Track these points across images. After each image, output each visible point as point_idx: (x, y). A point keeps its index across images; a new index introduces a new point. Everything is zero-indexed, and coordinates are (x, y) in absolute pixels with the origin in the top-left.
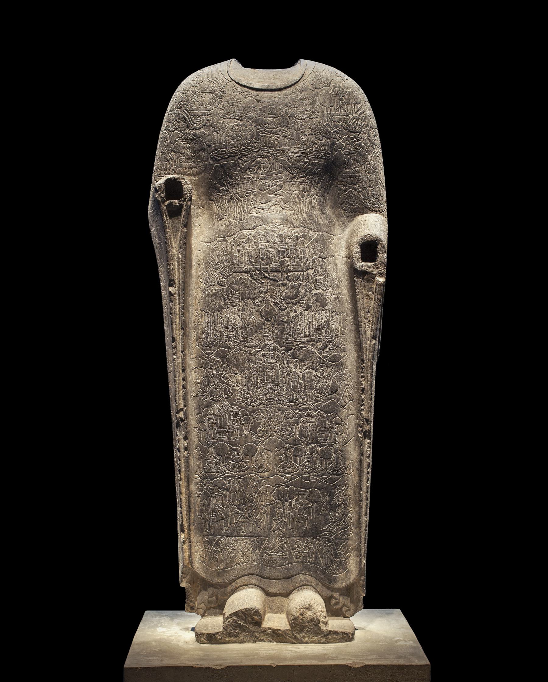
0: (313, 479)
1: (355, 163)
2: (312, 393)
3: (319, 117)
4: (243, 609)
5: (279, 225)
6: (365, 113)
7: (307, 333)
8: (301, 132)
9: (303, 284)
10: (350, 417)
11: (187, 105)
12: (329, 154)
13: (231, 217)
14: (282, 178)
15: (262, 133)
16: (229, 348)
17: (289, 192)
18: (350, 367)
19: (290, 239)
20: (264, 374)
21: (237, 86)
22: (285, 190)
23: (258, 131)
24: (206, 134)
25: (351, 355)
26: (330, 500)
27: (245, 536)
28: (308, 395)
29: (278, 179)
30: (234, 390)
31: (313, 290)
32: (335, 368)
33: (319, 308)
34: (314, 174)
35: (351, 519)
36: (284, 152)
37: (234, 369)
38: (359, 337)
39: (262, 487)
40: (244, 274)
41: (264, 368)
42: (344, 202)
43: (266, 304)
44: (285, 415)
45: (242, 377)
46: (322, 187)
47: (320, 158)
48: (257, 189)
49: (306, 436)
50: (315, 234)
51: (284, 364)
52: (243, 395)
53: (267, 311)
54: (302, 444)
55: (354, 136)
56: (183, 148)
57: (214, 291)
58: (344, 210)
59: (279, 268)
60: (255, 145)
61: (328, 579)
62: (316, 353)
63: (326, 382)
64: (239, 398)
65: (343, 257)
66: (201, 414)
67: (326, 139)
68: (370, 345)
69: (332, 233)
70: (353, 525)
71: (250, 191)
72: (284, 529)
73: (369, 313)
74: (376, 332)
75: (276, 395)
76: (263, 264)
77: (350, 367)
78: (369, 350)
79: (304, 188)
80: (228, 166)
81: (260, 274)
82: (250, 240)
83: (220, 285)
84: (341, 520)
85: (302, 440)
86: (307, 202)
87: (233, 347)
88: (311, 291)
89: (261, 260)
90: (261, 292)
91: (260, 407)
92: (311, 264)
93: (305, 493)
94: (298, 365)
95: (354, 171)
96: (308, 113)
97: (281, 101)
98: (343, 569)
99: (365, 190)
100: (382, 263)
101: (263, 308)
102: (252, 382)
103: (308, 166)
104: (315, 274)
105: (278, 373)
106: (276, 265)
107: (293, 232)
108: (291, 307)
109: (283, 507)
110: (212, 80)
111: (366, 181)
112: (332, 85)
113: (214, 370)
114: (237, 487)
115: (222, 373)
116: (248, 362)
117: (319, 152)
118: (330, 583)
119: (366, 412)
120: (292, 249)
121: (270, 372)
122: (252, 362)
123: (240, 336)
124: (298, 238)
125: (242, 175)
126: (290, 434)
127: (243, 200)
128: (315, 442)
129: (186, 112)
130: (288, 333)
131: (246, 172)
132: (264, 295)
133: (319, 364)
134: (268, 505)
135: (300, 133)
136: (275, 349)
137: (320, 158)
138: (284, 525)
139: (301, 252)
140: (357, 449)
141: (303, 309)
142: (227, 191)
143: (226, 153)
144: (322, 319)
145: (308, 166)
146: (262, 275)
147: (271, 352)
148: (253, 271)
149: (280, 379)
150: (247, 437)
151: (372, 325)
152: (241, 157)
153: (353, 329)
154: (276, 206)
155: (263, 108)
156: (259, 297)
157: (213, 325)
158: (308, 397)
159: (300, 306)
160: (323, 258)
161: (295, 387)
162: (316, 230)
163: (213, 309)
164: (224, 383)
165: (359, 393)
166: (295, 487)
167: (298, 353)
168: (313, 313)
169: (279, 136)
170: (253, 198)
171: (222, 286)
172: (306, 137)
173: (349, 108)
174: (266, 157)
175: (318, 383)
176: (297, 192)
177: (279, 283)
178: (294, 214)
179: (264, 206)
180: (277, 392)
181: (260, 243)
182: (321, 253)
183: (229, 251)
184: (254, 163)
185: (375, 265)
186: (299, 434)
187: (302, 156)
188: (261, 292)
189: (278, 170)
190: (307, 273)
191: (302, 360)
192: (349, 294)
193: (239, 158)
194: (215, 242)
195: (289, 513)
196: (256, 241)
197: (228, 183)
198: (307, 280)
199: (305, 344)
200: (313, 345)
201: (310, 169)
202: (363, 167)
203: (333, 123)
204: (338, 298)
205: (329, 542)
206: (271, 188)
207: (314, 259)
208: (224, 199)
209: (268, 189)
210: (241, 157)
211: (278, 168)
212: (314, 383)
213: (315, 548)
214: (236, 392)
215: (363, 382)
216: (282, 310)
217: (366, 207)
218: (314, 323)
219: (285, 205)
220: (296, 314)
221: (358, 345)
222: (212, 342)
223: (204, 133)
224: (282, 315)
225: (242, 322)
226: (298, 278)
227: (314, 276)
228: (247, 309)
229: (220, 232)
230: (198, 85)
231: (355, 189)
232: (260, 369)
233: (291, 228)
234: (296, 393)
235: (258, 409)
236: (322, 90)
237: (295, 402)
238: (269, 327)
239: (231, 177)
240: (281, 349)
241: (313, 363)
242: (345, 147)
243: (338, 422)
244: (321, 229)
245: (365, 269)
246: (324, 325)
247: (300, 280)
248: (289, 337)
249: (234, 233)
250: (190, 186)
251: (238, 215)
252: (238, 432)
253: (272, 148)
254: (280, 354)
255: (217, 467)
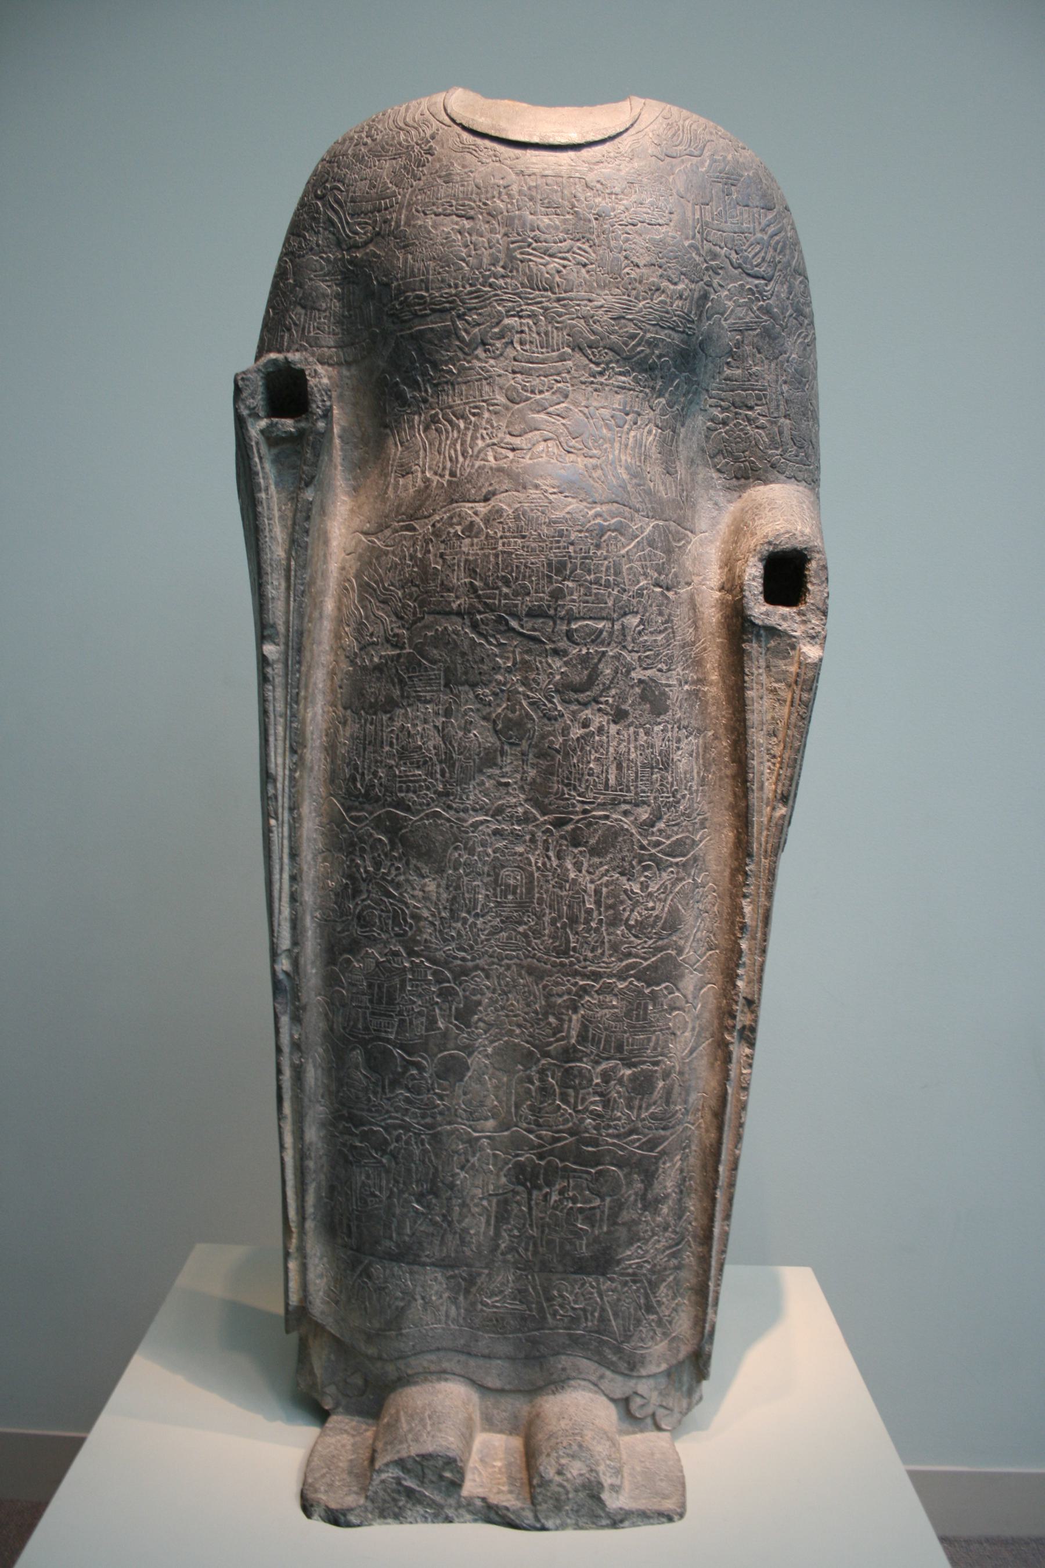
0: (608, 1144)
1: (754, 355)
2: (617, 935)
3: (672, 224)
4: (418, 1456)
5: (554, 493)
6: (783, 234)
7: (612, 782)
8: (626, 258)
9: (611, 654)
10: (705, 989)
11: (339, 189)
12: (693, 322)
13: (430, 468)
14: (569, 372)
15: (522, 253)
16: (408, 809)
17: (586, 410)
18: (715, 867)
19: (580, 531)
20: (496, 881)
21: (465, 135)
22: (576, 404)
23: (512, 246)
24: (379, 257)
25: (720, 837)
26: (646, 1190)
27: (433, 1264)
28: (606, 940)
29: (558, 374)
30: (417, 917)
31: (634, 669)
32: (678, 873)
33: (647, 716)
34: (652, 368)
35: (690, 1223)
36: (578, 305)
37: (419, 864)
38: (746, 796)
39: (478, 1155)
40: (455, 619)
41: (497, 867)
42: (720, 452)
43: (508, 700)
44: (545, 987)
45: (439, 886)
46: (670, 404)
47: (669, 328)
48: (501, 399)
49: (595, 1041)
50: (648, 524)
51: (549, 858)
52: (440, 931)
53: (510, 720)
54: (585, 1059)
55: (756, 286)
56: (325, 296)
57: (376, 660)
58: (719, 471)
59: (549, 606)
60: (501, 282)
61: (629, 1363)
62: (632, 835)
63: (653, 909)
64: (428, 938)
65: (712, 589)
66: (335, 964)
67: (686, 281)
68: (771, 818)
69: (688, 525)
70: (694, 1237)
71: (483, 401)
72: (529, 1254)
73: (775, 736)
74: (791, 785)
75: (525, 935)
76: (506, 595)
77: (715, 867)
78: (768, 830)
79: (625, 404)
80: (430, 335)
81: (495, 621)
82: (475, 530)
83: (392, 645)
84: (665, 1229)
85: (583, 1051)
86: (631, 440)
87: (419, 807)
88: (628, 672)
89: (500, 584)
90: (496, 669)
91: (481, 962)
92: (634, 601)
93: (585, 1176)
94: (586, 865)
95: (750, 375)
96: (644, 210)
97: (577, 175)
98: (664, 1334)
99: (775, 423)
100: (818, 609)
101: (499, 710)
102: (464, 899)
103: (638, 344)
104: (642, 627)
105: (532, 882)
106: (541, 599)
107: (591, 513)
108: (574, 713)
109: (529, 1204)
110: (403, 126)
111: (778, 401)
112: (707, 153)
113: (368, 863)
114: (417, 1152)
115: (389, 871)
116: (456, 848)
117: (667, 313)
118: (632, 1370)
119: (749, 982)
120: (585, 558)
121: (511, 876)
122: (465, 848)
123: (436, 780)
124: (603, 531)
125: (465, 360)
126: (554, 1034)
127: (462, 425)
128: (618, 1055)
129: (335, 206)
130: (563, 781)
131: (476, 352)
132: (505, 678)
133: (640, 862)
134: (490, 1195)
135: (622, 258)
136: (526, 819)
137: (669, 328)
138: (527, 1244)
139: (608, 568)
140: (717, 1069)
141: (606, 717)
142: (425, 401)
143: (425, 302)
144: (653, 746)
145: (638, 344)
146: (501, 623)
147: (516, 827)
148: (480, 613)
149: (537, 895)
150: (445, 1035)
151: (781, 768)
152: (464, 314)
153: (728, 772)
154: (550, 443)
155: (529, 189)
156: (490, 682)
157: (370, 748)
158: (607, 945)
159: (600, 710)
160: (665, 586)
161: (573, 920)
162: (651, 514)
163: (371, 706)
164: (393, 896)
165: (734, 935)
166: (562, 1161)
167: (586, 832)
168: (632, 729)
169: (565, 262)
170: (489, 421)
171: (395, 646)
172: (638, 270)
173: (746, 216)
174: (529, 316)
175: (632, 911)
176: (606, 413)
177: (548, 647)
178: (595, 467)
179: (517, 441)
180: (525, 927)
181: (501, 537)
182: (660, 574)
183: (419, 555)
184: (496, 330)
185: (799, 613)
186: (578, 1036)
187: (624, 318)
188: (496, 669)
189: (558, 350)
190: (623, 625)
191: (594, 852)
192: (724, 682)
193: (460, 317)
194: (388, 532)
195: (542, 1218)
196: (491, 533)
197: (429, 381)
198: (620, 643)
199: (606, 810)
200: (625, 813)
201: (642, 355)
202: (773, 365)
203: (707, 246)
204: (696, 693)
205: (635, 1282)
206: (538, 397)
207: (642, 589)
208: (416, 422)
209: (528, 399)
210: (464, 314)
211: (558, 345)
212: (624, 910)
213: (602, 1299)
214: (422, 923)
215: (747, 909)
216: (549, 719)
217: (773, 466)
218: (633, 756)
219: (573, 443)
220: (587, 730)
221: (739, 816)
222: (366, 791)
223: (375, 255)
224: (550, 733)
225: (443, 746)
226: (596, 637)
227: (640, 633)
228: (458, 711)
229: (400, 506)
230: (369, 141)
231: (748, 419)
232: (486, 869)
233: (585, 504)
234: (577, 933)
235: (477, 968)
236: (683, 162)
237: (572, 956)
238: (515, 763)
239: (435, 366)
240: (542, 819)
241: (623, 859)
242: (732, 311)
243: (678, 1005)
244: (663, 512)
245: (772, 621)
246: (657, 762)
247: (602, 643)
248: (566, 790)
249: (434, 510)
250: (325, 381)
251: (448, 464)
252: (422, 1023)
253: (546, 293)
254: (540, 834)
255: (369, 1100)
